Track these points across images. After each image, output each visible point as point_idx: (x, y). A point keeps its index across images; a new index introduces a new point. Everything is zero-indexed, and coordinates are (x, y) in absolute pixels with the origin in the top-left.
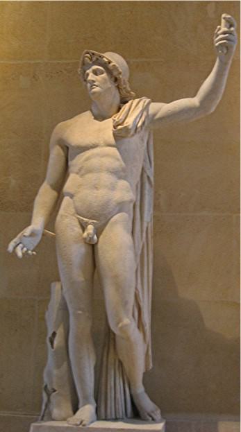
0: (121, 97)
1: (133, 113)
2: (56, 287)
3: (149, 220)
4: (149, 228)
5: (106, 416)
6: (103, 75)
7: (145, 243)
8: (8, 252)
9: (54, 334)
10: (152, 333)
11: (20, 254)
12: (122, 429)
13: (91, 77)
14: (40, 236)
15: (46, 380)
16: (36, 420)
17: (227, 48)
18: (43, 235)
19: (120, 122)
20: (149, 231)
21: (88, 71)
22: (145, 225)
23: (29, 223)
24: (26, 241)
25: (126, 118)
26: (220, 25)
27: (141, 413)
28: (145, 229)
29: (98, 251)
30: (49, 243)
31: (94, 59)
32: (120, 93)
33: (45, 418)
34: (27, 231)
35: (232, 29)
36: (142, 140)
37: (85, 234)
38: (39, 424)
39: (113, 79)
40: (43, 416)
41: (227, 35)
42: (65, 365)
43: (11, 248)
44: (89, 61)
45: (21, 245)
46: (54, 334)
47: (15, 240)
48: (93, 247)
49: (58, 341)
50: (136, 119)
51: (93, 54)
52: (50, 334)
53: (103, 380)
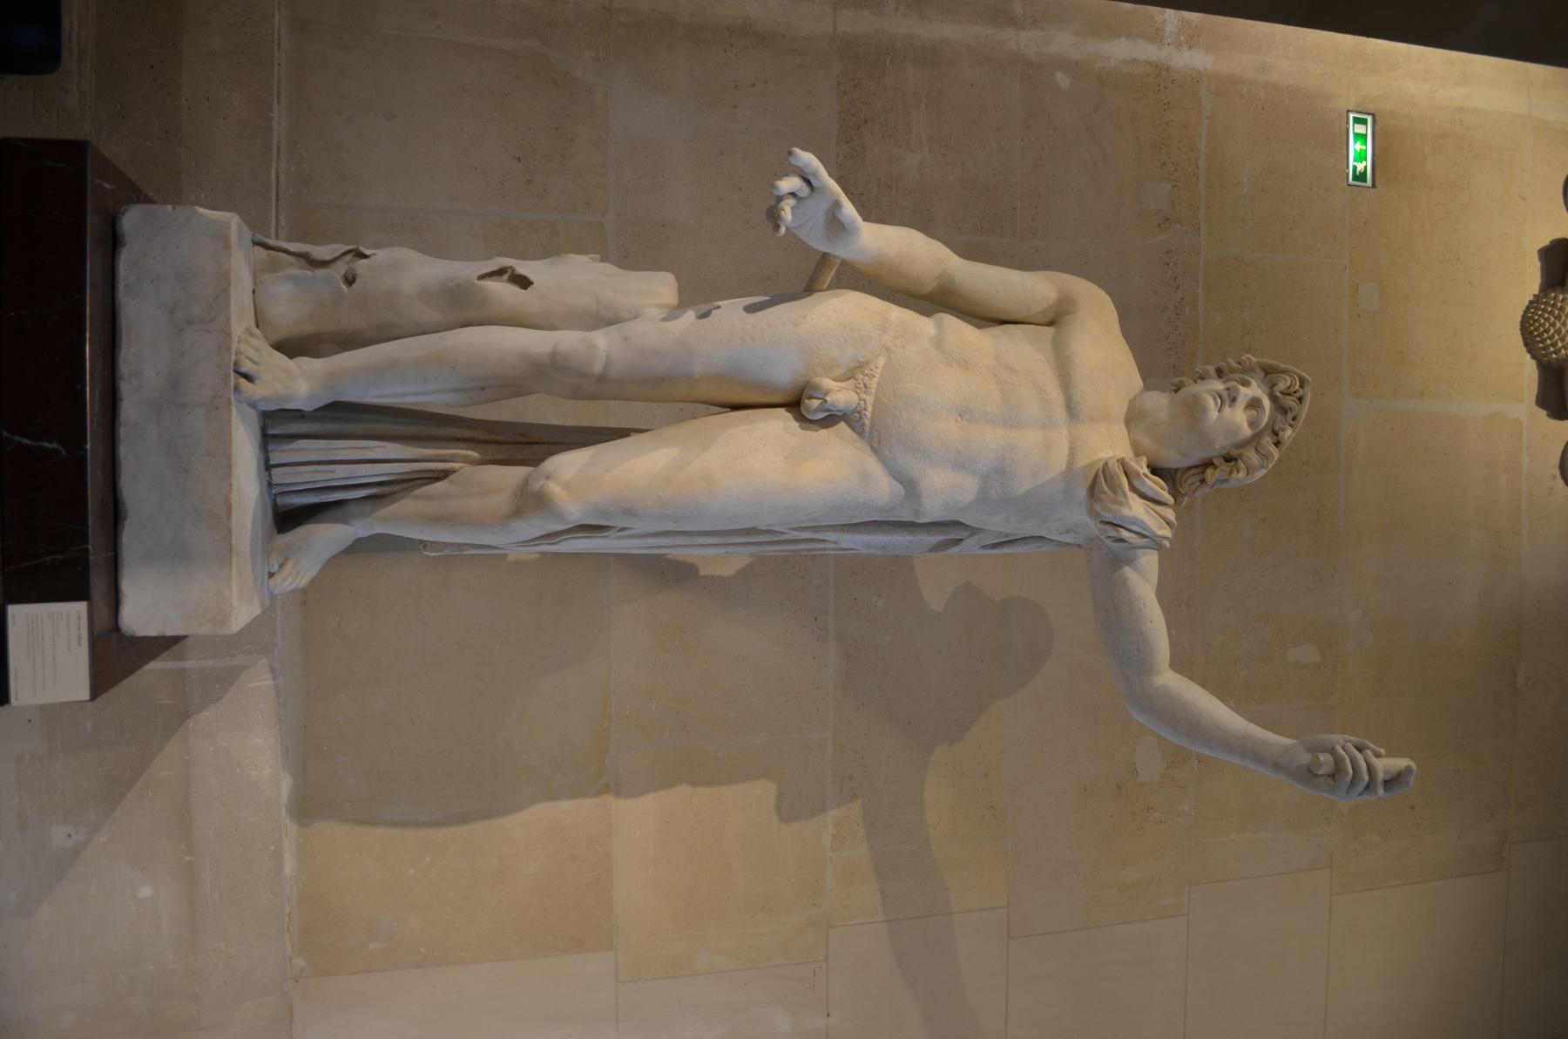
1: (1145, 513)
2: (662, 287)
3: (843, 545)
4: (822, 546)
5: (274, 436)
6: (1245, 425)
7: (783, 538)
8: (773, 186)
9: (524, 282)
12: (115, 513)
13: (1246, 393)
14: (821, 247)
15: (380, 256)
16: (255, 222)
17: (1332, 776)
20: (817, 546)
22: (831, 536)
25: (1143, 496)
26: (1389, 755)
27: (290, 536)
31: (1290, 402)
32: (1189, 468)
33: (261, 253)
34: (849, 210)
35: (1381, 791)
37: (827, 382)
38: (234, 239)
39: (1234, 452)
40: (267, 247)
41: (1366, 778)
42: (434, 316)
43: (807, 159)
45: (803, 190)
46: (524, 282)
49: (501, 289)
51: (1300, 399)
52: (523, 268)
53: (401, 429)
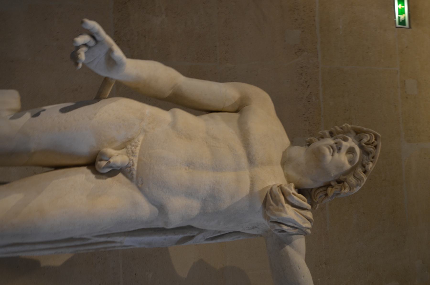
0: (312, 189)
4: (113, 245)
7: (89, 242)
8: (73, 41)
10: (64, 102)
11: (82, 39)
13: (346, 145)
14: (104, 74)
18: (106, 80)
19: (289, 199)
21: (350, 139)
22: (118, 239)
23: (130, 55)
24: (100, 53)
25: (293, 206)
28: (110, 239)
29: (103, 179)
30: (100, 89)
31: (370, 148)
36: (253, 228)
37: (110, 151)
39: (342, 178)
43: (93, 25)
44: (365, 140)
45: (92, 43)
47: (102, 33)
48: (350, 190)
50: (290, 220)
51: (376, 147)
